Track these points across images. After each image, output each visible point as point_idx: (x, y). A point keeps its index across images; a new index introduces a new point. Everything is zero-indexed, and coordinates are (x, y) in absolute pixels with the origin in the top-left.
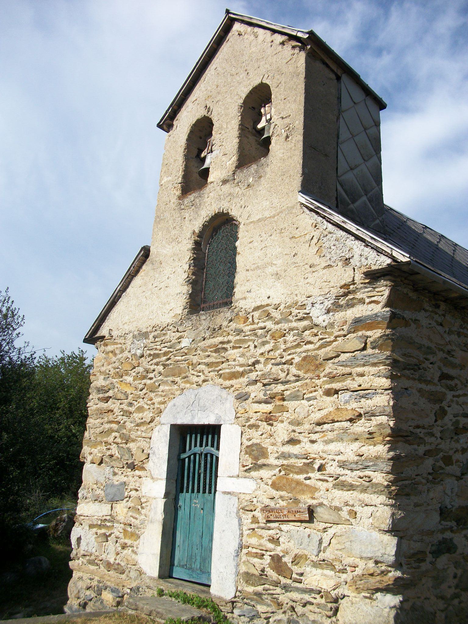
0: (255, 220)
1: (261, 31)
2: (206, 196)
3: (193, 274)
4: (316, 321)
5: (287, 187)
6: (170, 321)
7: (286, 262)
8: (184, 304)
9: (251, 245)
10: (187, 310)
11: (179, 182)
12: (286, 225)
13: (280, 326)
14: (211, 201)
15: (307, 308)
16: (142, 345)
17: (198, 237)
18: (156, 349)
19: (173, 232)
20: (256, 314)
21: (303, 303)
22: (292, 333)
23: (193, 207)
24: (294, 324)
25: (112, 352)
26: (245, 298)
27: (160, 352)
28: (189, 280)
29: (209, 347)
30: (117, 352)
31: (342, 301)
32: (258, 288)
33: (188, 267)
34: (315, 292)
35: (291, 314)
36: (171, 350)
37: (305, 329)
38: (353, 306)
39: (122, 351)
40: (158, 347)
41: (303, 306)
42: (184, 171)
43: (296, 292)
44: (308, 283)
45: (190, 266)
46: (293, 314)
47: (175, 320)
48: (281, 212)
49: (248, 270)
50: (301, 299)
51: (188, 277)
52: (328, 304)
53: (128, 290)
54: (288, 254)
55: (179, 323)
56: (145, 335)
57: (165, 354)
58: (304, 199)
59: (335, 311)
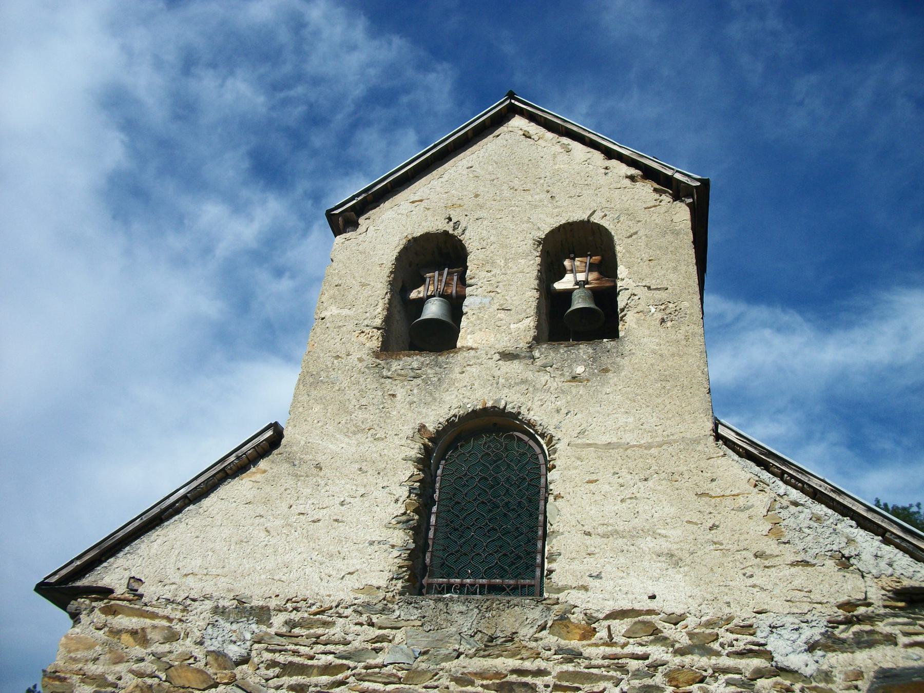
0: (600, 443)
1: (576, 146)
2: (457, 369)
4: (780, 660)
5: (678, 403)
6: (349, 598)
7: (692, 537)
8: (394, 568)
9: (592, 486)
10: (400, 584)
12: (683, 468)
13: (687, 660)
15: (759, 634)
16: (248, 636)
17: (430, 439)
18: (295, 653)
19: (360, 415)
20: (620, 627)
21: (746, 623)
22: (722, 678)
23: (419, 381)
24: (725, 661)
25: (134, 633)
26: (585, 588)
27: (310, 662)
28: (408, 521)
29: (482, 675)
30: (152, 635)
31: (843, 631)
32: (622, 574)
34: (777, 605)
35: (717, 639)
36: (351, 664)
37: (759, 674)
38: (870, 645)
39: (172, 637)
40: (303, 650)
41: (747, 629)
44: (754, 586)
45: (410, 493)
46: (721, 640)
47: (363, 598)
48: (670, 443)
49: (589, 534)
50: (742, 614)
52: (815, 633)
53: (206, 502)
54: (696, 524)
55: (379, 606)
56: (262, 614)
57: (327, 669)
58: (733, 434)
59: (827, 648)
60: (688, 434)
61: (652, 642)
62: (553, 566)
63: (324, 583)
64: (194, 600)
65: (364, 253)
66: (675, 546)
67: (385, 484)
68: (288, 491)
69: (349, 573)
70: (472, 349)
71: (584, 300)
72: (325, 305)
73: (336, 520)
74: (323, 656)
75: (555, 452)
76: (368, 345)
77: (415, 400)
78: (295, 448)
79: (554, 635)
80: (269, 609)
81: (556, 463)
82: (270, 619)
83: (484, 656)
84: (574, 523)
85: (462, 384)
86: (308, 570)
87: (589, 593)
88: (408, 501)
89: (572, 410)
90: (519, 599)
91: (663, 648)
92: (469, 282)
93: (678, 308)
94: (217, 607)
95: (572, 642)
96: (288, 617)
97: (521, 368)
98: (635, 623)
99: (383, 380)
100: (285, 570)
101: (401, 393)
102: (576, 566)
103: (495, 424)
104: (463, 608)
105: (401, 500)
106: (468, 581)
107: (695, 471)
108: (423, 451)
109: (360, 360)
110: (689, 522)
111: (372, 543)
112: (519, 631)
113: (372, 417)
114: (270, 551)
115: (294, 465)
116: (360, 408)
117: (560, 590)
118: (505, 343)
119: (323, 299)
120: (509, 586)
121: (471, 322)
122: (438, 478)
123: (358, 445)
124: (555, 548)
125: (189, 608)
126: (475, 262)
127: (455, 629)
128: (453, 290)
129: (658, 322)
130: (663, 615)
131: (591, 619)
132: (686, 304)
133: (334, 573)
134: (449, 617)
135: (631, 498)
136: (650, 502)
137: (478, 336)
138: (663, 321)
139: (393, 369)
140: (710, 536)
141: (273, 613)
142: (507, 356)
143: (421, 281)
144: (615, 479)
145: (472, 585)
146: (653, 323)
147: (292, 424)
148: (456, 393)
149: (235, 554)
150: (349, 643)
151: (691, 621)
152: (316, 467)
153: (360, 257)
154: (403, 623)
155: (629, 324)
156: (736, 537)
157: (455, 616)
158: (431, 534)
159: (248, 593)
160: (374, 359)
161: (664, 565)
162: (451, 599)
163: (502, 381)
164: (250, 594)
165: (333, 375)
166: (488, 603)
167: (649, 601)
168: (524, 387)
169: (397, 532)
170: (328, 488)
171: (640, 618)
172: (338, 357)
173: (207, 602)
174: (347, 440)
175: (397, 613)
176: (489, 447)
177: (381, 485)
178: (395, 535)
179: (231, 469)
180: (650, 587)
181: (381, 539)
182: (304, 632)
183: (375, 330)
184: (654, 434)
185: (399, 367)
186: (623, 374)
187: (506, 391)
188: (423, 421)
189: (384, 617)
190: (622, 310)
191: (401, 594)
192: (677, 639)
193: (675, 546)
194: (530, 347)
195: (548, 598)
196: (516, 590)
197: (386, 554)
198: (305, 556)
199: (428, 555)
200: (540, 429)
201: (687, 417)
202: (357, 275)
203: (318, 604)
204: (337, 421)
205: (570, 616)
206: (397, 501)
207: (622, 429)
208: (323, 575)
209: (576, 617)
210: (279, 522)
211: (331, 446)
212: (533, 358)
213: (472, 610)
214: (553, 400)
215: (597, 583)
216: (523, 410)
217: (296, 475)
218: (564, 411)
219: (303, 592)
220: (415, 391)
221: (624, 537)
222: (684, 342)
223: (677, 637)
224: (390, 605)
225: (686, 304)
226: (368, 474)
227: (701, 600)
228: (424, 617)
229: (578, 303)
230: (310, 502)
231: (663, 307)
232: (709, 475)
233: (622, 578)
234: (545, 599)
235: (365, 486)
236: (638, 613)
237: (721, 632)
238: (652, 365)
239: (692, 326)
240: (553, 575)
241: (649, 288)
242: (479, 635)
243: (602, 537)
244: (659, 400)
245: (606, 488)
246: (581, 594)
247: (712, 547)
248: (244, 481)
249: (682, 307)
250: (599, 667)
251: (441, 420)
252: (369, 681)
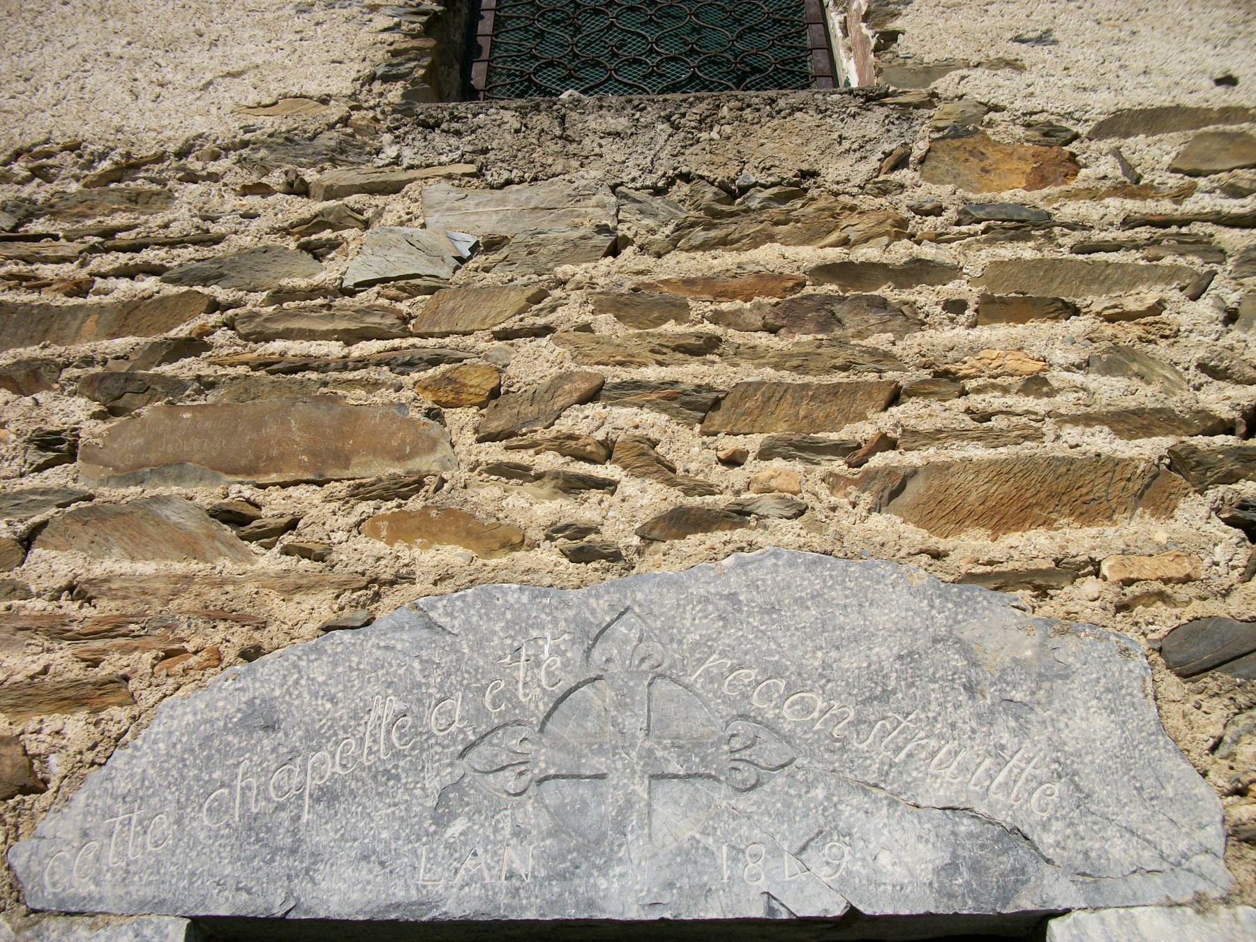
6: (225, 128)
8: (380, 55)
20: (1155, 153)
26: (1015, 65)
36: (220, 293)
74: (124, 284)
83: (705, 246)
104: (621, 123)
134: (572, 148)
150: (218, 240)
166: (703, 106)
180: (1210, 61)
182: (60, 227)
203: (121, 150)
215: (1041, 52)
219: (69, 127)
228: (485, 151)
250: (1116, 247)
252: (287, 335)
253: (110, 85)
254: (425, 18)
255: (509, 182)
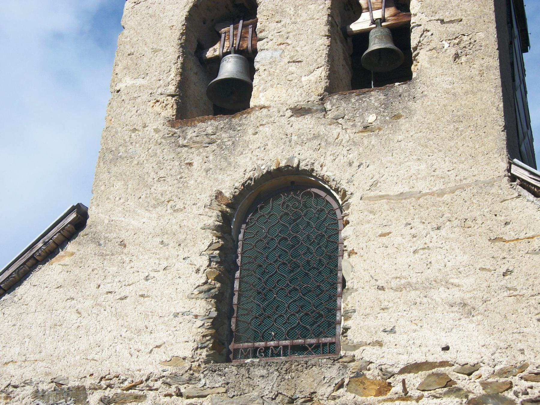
2: (251, 131)
3: (217, 279)
5: (471, 144)
6: (157, 371)
7: (486, 284)
8: (198, 338)
9: (384, 239)
10: (204, 353)
11: (168, 92)
14: (261, 143)
17: (228, 205)
19: (159, 188)
20: (414, 380)
23: (214, 147)
26: (380, 344)
28: (209, 290)
32: (415, 327)
33: (207, 263)
35: (511, 387)
42: (181, 74)
43: (520, 346)
45: (210, 261)
46: (515, 388)
47: (171, 370)
48: (462, 188)
49: (382, 288)
51: (206, 283)
53: (20, 290)
54: (489, 270)
55: (186, 377)
58: (527, 173)
60: (482, 176)
61: (445, 394)
62: (349, 323)
63: (134, 358)
64: (15, 387)
65: (154, 16)
66: (468, 295)
67: (186, 255)
68: (96, 272)
69: (157, 347)
70: (264, 107)
71: (381, 39)
72: (119, 76)
73: (142, 296)
75: (348, 208)
76: (163, 114)
77: (211, 166)
78: (99, 227)
79: (351, 392)
80: (84, 388)
81: (350, 218)
82: (86, 398)
84: (367, 278)
85: (256, 145)
86: (119, 347)
87: (384, 349)
88: (208, 270)
89: (364, 162)
90: (316, 359)
91: (457, 399)
92: (260, 35)
93: (472, 41)
94: (37, 391)
95: (369, 398)
96: (102, 394)
97: (313, 122)
98: (429, 376)
99: (179, 149)
100: (98, 349)
101: (197, 161)
102: (370, 322)
103: (293, 183)
104: (264, 372)
105: (202, 269)
106: (272, 343)
107: (488, 215)
108: (220, 218)
109: (157, 131)
110: (482, 269)
111: (176, 315)
112: (317, 390)
113: (170, 188)
114: (82, 332)
115: (100, 245)
116: (159, 181)
117: (355, 347)
118: (297, 98)
119: (117, 71)
120: (310, 345)
121: (263, 79)
122: (240, 243)
123: (159, 218)
124: (350, 306)
125: (12, 395)
126: (265, 13)
127: (256, 394)
128: (247, 44)
129: (451, 58)
130: (456, 365)
131: (387, 374)
132: (481, 35)
133: (142, 348)
135: (423, 249)
136: (443, 251)
137: (270, 92)
138: (457, 56)
139: (189, 137)
140: (504, 282)
141: (89, 392)
142: (299, 111)
143: (216, 38)
144: (407, 231)
145: (276, 347)
146: (447, 59)
147: (95, 203)
148: (250, 155)
149: (50, 338)
151: (485, 371)
152: (120, 245)
153: (151, 21)
154: (209, 391)
155: (422, 63)
156: (531, 280)
157: (257, 381)
158: (235, 300)
159: (64, 375)
160: (170, 129)
161: (458, 316)
162: (253, 364)
163: (294, 138)
164: (66, 375)
165: (131, 149)
166: (287, 365)
167: (442, 352)
168: (316, 142)
169: (199, 301)
170: (132, 264)
171: (434, 370)
172: (135, 130)
173: (27, 387)
174: (148, 214)
175: (203, 382)
176: (288, 206)
177: (182, 257)
178: (197, 305)
179: (40, 255)
181: (185, 310)
183: (170, 98)
184: (447, 180)
185: (195, 134)
186: (415, 119)
187: (299, 148)
188: (219, 188)
189: (191, 386)
190: (415, 49)
191: (206, 362)
192: (471, 389)
193: (468, 295)
194: (322, 99)
195: (345, 356)
196: (318, 349)
197: (190, 325)
198: (114, 333)
199: (233, 320)
200: (333, 184)
201: (480, 158)
202: (148, 41)
203: (130, 380)
204: (138, 196)
205: (365, 372)
206: (198, 271)
207: (414, 177)
208: (133, 351)
209: (372, 374)
210: (89, 303)
211: (133, 222)
212: (325, 110)
213: (272, 373)
214: (345, 153)
216: (317, 167)
217: (102, 255)
218: (356, 164)
219: (115, 369)
220: (211, 158)
221: (416, 289)
222: (478, 78)
223: (471, 387)
224: (196, 375)
225: (481, 35)
226: (170, 246)
227: (494, 349)
228: (228, 383)
229: (375, 45)
230: (117, 280)
231: (456, 41)
232: (503, 218)
233: (415, 331)
234: (341, 357)
235: (167, 259)
236: (432, 365)
237: (515, 380)
238: (445, 106)
239: (487, 59)
240: (349, 333)
241: (442, 21)
242: (280, 397)
243: (396, 290)
244: (452, 144)
245: (398, 240)
246: (376, 350)
247: (506, 294)
248: (53, 266)
249: (477, 38)
251: (237, 185)
253: (124, 350)
254: (211, 320)
255: (234, 396)
